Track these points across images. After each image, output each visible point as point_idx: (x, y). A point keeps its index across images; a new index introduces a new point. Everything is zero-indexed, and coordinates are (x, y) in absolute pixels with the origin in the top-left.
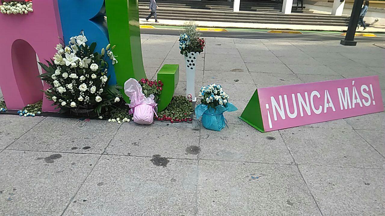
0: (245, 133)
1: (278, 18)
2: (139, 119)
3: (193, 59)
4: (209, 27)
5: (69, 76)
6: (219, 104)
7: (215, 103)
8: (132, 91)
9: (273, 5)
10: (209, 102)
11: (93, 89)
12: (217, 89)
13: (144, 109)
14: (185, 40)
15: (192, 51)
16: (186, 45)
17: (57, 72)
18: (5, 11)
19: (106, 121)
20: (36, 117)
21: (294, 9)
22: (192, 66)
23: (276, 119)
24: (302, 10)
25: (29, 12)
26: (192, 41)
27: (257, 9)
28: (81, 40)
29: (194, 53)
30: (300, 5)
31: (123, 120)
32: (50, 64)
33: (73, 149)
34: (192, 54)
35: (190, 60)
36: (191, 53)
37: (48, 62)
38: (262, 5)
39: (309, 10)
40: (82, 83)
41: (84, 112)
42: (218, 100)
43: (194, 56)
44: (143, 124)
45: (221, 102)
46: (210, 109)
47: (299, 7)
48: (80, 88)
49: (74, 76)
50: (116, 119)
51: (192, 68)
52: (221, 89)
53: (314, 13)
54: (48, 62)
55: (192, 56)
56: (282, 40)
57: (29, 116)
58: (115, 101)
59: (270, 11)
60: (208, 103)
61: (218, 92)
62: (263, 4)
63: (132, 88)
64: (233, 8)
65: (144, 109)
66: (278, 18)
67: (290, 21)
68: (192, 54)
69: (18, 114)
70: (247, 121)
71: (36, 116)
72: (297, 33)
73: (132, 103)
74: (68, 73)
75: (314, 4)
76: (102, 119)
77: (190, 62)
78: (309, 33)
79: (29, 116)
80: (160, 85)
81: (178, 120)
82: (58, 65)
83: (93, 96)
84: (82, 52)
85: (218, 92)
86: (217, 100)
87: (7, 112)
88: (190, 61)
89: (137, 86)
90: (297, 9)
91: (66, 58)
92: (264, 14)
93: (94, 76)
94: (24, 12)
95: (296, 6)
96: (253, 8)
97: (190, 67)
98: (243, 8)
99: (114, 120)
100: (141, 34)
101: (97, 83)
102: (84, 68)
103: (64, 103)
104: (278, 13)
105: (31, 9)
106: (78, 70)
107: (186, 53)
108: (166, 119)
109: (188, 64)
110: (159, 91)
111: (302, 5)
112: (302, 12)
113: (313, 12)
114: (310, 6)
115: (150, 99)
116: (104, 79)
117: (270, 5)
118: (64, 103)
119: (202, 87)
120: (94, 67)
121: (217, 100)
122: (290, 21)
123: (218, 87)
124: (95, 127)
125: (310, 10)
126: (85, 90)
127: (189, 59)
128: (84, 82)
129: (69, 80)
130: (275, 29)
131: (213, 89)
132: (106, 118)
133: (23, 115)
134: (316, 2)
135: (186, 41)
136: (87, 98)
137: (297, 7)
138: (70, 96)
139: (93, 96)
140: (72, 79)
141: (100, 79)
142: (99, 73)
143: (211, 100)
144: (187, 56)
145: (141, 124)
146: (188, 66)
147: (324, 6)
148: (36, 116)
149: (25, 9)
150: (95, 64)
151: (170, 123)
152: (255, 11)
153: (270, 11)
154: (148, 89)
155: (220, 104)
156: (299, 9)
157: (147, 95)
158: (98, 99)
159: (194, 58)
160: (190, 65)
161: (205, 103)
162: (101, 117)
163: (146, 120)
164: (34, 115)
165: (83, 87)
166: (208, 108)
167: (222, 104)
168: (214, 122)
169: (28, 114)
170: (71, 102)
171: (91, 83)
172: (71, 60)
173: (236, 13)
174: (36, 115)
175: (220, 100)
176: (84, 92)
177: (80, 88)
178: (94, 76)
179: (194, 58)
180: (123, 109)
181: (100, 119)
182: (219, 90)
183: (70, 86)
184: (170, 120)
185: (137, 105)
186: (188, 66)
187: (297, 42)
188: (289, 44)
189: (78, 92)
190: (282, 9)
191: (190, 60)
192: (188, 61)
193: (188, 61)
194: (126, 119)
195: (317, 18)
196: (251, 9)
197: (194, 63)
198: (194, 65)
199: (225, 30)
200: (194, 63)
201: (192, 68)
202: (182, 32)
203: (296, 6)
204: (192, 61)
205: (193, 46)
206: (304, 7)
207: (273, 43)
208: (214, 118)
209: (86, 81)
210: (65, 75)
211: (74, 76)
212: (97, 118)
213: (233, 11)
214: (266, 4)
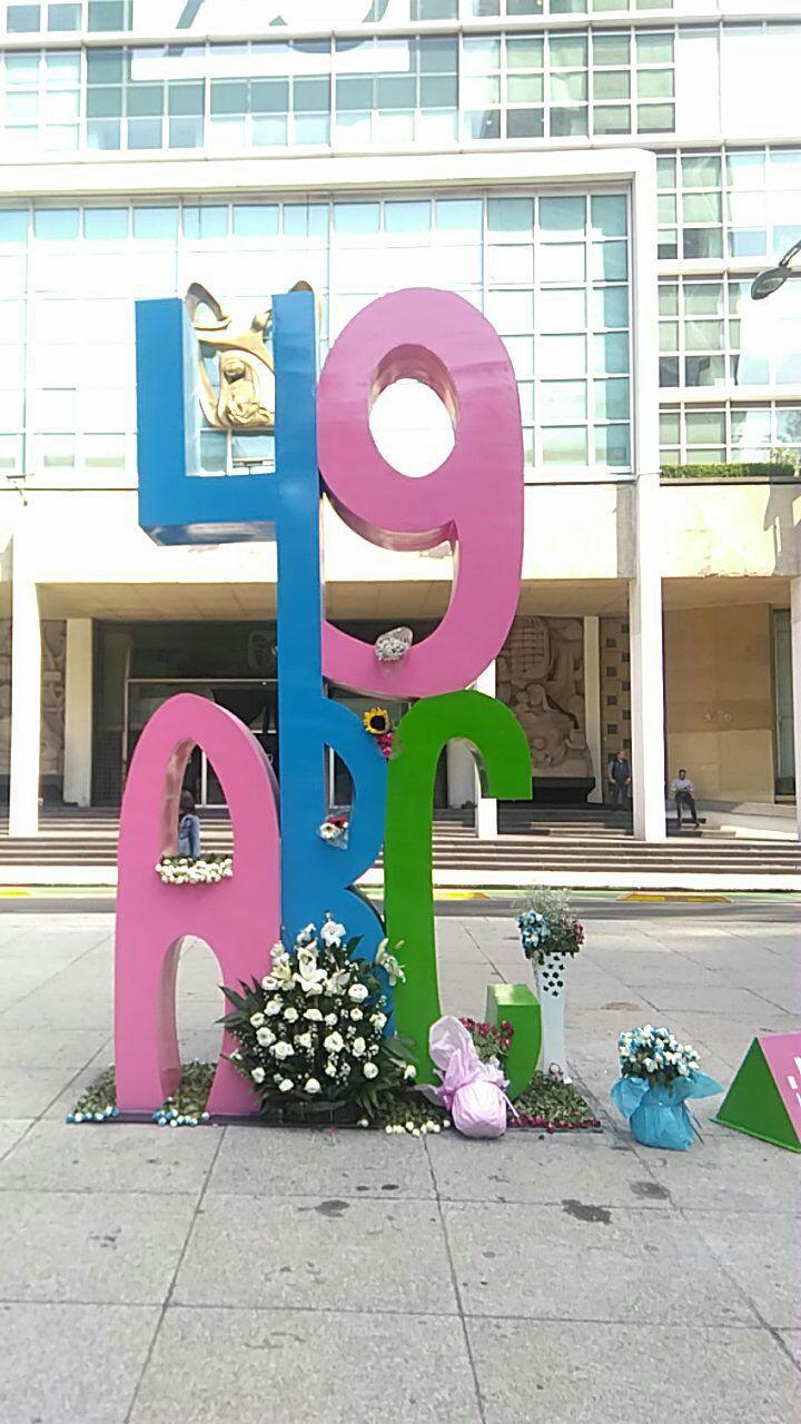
0: (744, 1154)
1: (628, 853)
2: (477, 1120)
3: (559, 971)
4: (75, 886)
5: (305, 1015)
6: (678, 1074)
7: (670, 1071)
8: (447, 1047)
9: (598, 815)
10: (655, 1070)
11: (359, 1044)
12: (662, 1039)
13: (481, 1095)
14: (536, 924)
15: (554, 951)
16: (540, 937)
17: (273, 1007)
18: (172, 879)
19: (379, 1134)
20: (201, 1127)
21: (673, 828)
22: (556, 988)
24: (696, 828)
25: (225, 878)
26: (555, 928)
27: (552, 829)
28: (333, 933)
29: (559, 955)
30: (687, 815)
31: (424, 1128)
32: (248, 991)
33: (360, 1189)
34: (556, 958)
35: (551, 972)
36: (553, 954)
37: (243, 984)
38: (564, 818)
39: (719, 828)
40: (332, 1032)
41: (322, 1110)
42: (677, 1065)
43: (559, 963)
44: (483, 1135)
45: (683, 1069)
46: (655, 1089)
47: (686, 821)
48: (328, 1043)
49: (314, 1014)
50: (403, 1125)
51: (555, 994)
52: (672, 1037)
53: (737, 836)
54: (243, 984)
55: (554, 962)
56: (691, 923)
57: (184, 1124)
58: (406, 1077)
59: (591, 833)
60: (651, 1071)
61: (667, 1045)
62: (584, 814)
63: (449, 1042)
64: (473, 826)
65: (481, 1095)
66: (628, 853)
67: (671, 862)
68: (556, 958)
69: (155, 1122)
70: (742, 1129)
71: (199, 1124)
72: (715, 899)
73: (450, 1078)
74: (297, 1009)
75: (733, 808)
76: (368, 1128)
77: (551, 978)
78: (755, 898)
79: (184, 1124)
80: (506, 1033)
81: (566, 1125)
82: (274, 992)
83: (357, 1064)
84: (329, 959)
85: (667, 1045)
86: (674, 1063)
87: (121, 1118)
88: (551, 975)
89: (460, 1035)
90: (679, 826)
91: (299, 973)
92: (581, 845)
93: (357, 1015)
94: (213, 878)
95: (676, 817)
96: (535, 826)
97: (552, 989)
98: (508, 826)
99: (399, 1129)
100: (436, 918)
101: (365, 1028)
102: (335, 996)
103: (286, 1085)
104: (619, 837)
105: (229, 872)
106: (323, 1001)
107: (541, 956)
108: (530, 1122)
109: (545, 982)
110: (504, 1048)
111: (694, 814)
112: (699, 835)
113: (734, 833)
114: (722, 817)
115: (491, 1067)
116: (379, 1020)
117: (591, 817)
118: (286, 1085)
119: (622, 1034)
120: (359, 992)
121: (674, 1063)
122: (671, 862)
123: (662, 1031)
124: (364, 1144)
125: (724, 829)
126: (338, 1050)
127: (548, 971)
128: (335, 1027)
129: (303, 1025)
130: (636, 889)
131: (653, 1038)
132: (376, 1125)
133: (168, 1122)
134: (736, 804)
135: (540, 926)
136: (346, 1068)
137: (678, 819)
138: (299, 1065)
139: (357, 1064)
140: (309, 1022)
141: (371, 1020)
142: (368, 1007)
143: (659, 1064)
144: (541, 963)
145: (474, 1135)
146: (546, 989)
147: (766, 816)
148: (199, 1124)
149: (217, 871)
150: (360, 986)
151: (545, 1134)
152: (546, 833)
153: (591, 833)
154: (482, 1043)
155: (681, 1073)
156: (685, 827)
157: (485, 1058)
158: (370, 1070)
159: (561, 967)
160: (551, 984)
161: (643, 1072)
162: (365, 1122)
163: (493, 1123)
164: (195, 1121)
165: (334, 1042)
166: (650, 1085)
167: (687, 1074)
168: (669, 1123)
169: (181, 1119)
170: (307, 1080)
171: (352, 1030)
172: (312, 979)
173: (489, 843)
174: (201, 1122)
175: (680, 1063)
176: (336, 1053)
177: (328, 1043)
178: (357, 1015)
179: (561, 967)
180: (423, 1102)
181: (362, 1127)
182: (666, 1041)
183: (305, 1040)
184: (544, 1125)
185: (462, 1085)
186: (546, 989)
187: (742, 927)
188: (722, 933)
189: (323, 1054)
190: (632, 827)
191: (551, 972)
192: (546, 975)
193: (546, 975)
194: (430, 1124)
195: (757, 851)
196: (532, 828)
197: (560, 979)
198: (560, 984)
199: (480, 894)
200: (560, 979)
201: (555, 994)
202: (520, 904)
203: (676, 817)
204: (556, 975)
205: (555, 939)
206: (704, 821)
207: (674, 932)
208: (668, 1114)
209: (342, 1026)
210: (291, 1014)
211: (314, 1014)
212: (352, 1125)
213: (477, 837)
214: (577, 814)
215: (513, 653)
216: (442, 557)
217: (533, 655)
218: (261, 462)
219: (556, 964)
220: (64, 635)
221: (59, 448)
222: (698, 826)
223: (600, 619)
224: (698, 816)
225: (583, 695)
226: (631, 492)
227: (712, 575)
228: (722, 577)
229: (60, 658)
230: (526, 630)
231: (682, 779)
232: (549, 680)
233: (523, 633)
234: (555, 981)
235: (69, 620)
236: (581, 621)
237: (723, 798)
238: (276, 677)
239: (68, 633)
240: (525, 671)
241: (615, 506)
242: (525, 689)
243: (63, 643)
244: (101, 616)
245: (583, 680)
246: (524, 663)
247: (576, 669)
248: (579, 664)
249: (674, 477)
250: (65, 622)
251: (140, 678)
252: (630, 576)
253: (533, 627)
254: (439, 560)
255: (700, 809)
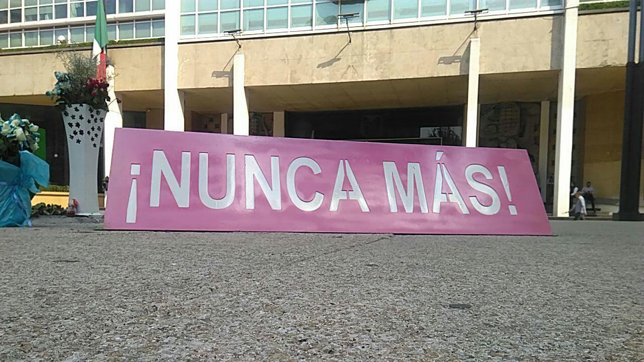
3: (79, 121)
23: (155, 202)
29: (78, 106)
34: (77, 110)
36: (74, 106)
51: (78, 141)
55: (75, 113)
88: (74, 125)
111: (593, 206)
146: (72, 137)
191: (74, 122)
197: (81, 128)
200: (81, 128)
201: (78, 141)
204: (78, 125)
206: (599, 210)
215: (500, 122)
216: (451, 63)
217: (511, 123)
218: (352, 15)
219: (77, 114)
220: (273, 120)
221: (255, 16)
222: (595, 212)
223: (551, 103)
224: (596, 207)
225: (539, 145)
226: (561, 20)
227: (607, 66)
228: (614, 67)
229: (271, 131)
230: (508, 109)
231: (588, 187)
232: (520, 137)
233: (506, 111)
234: (78, 130)
235: (275, 113)
236: (540, 104)
237: (613, 198)
238: (164, 35)
239: (274, 119)
240: (506, 132)
241: (551, 29)
242: (505, 142)
243: (272, 123)
244: (289, 109)
245: (539, 136)
246: (506, 128)
247: (535, 130)
248: (537, 128)
249: (589, 9)
250: (273, 113)
251: (16, 7)
252: (558, 69)
253: (512, 108)
254: (450, 65)
255: (597, 203)
